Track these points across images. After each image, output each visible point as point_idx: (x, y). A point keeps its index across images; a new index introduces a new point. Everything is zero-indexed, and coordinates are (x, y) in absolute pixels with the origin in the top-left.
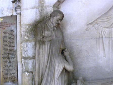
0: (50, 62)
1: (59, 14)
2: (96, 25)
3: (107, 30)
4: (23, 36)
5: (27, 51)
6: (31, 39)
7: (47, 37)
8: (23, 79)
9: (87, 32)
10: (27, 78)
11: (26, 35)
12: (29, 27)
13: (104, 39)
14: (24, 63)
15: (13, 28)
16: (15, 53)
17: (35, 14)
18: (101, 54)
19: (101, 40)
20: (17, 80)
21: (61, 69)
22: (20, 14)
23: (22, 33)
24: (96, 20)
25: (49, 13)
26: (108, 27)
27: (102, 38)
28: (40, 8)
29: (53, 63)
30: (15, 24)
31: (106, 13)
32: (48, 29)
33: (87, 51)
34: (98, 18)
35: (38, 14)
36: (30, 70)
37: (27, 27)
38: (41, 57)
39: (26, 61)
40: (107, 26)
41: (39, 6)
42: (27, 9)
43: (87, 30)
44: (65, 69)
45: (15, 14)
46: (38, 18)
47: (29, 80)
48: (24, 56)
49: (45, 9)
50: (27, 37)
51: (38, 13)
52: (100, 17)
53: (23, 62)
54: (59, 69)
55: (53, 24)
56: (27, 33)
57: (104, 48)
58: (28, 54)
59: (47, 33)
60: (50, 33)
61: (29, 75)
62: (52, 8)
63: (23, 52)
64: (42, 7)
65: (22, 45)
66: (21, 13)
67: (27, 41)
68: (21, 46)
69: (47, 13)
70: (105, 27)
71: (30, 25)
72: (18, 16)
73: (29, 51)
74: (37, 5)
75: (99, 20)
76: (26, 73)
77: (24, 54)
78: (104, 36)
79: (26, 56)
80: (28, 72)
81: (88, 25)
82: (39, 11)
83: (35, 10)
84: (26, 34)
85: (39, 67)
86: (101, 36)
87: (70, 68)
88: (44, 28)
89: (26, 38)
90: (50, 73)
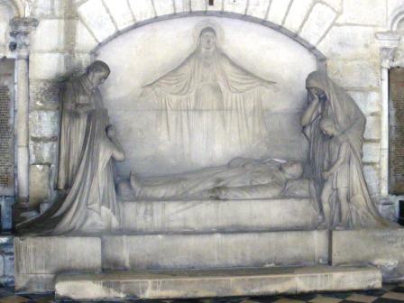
0: (89, 152)
1: (103, 69)
2: (158, 89)
3: (175, 98)
4: (32, 100)
5: (40, 127)
6: (49, 106)
7: (83, 105)
8: (32, 178)
9: (142, 99)
10: (39, 175)
11: (38, 99)
12: (45, 85)
13: (169, 112)
14: (35, 148)
15: (6, 83)
16: (10, 130)
17: (56, 62)
18: (164, 136)
19: (164, 112)
20: (391, 81)
21: (108, 157)
22: (28, 60)
23: (31, 94)
24: (157, 81)
25: (85, 66)
26: (176, 94)
27: (166, 110)
28: (67, 54)
29: (95, 147)
30: (10, 75)
31: (175, 71)
32: (84, 93)
33: (141, 130)
34: (161, 78)
35: (63, 65)
36: (45, 161)
37: (42, 85)
38: (72, 138)
39: (39, 145)
40: (176, 91)
41: (65, 49)
42: (41, 52)
43: (141, 95)
44: (113, 158)
45: (10, 55)
46: (63, 70)
47: (43, 178)
48: (34, 135)
49: (76, 55)
50: (42, 102)
51: (63, 60)
52: (165, 76)
53: (31, 147)
54: (289, 238)
55: (92, 84)
56: (42, 95)
57: (168, 127)
58: (42, 132)
59: (82, 99)
60: (87, 98)
61: (43, 170)
62: (89, 56)
63: (32, 129)
64: (71, 52)
65: (30, 117)
66: (30, 59)
67: (41, 109)
68: (28, 119)
69: (80, 64)
70: (172, 93)
71: (48, 81)
72: (20, 66)
73: (43, 126)
74: (62, 47)
75: (163, 81)
76: (38, 166)
77: (34, 131)
78: (168, 108)
79: (39, 136)
80: (41, 164)
81: (143, 87)
82: (66, 59)
83: (57, 55)
84: (39, 96)
85: (69, 153)
86: (164, 108)
87: (118, 156)
88: (79, 91)
89: (38, 103)
90: (90, 164)
